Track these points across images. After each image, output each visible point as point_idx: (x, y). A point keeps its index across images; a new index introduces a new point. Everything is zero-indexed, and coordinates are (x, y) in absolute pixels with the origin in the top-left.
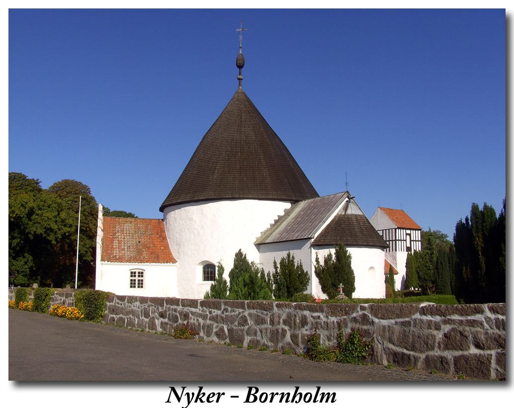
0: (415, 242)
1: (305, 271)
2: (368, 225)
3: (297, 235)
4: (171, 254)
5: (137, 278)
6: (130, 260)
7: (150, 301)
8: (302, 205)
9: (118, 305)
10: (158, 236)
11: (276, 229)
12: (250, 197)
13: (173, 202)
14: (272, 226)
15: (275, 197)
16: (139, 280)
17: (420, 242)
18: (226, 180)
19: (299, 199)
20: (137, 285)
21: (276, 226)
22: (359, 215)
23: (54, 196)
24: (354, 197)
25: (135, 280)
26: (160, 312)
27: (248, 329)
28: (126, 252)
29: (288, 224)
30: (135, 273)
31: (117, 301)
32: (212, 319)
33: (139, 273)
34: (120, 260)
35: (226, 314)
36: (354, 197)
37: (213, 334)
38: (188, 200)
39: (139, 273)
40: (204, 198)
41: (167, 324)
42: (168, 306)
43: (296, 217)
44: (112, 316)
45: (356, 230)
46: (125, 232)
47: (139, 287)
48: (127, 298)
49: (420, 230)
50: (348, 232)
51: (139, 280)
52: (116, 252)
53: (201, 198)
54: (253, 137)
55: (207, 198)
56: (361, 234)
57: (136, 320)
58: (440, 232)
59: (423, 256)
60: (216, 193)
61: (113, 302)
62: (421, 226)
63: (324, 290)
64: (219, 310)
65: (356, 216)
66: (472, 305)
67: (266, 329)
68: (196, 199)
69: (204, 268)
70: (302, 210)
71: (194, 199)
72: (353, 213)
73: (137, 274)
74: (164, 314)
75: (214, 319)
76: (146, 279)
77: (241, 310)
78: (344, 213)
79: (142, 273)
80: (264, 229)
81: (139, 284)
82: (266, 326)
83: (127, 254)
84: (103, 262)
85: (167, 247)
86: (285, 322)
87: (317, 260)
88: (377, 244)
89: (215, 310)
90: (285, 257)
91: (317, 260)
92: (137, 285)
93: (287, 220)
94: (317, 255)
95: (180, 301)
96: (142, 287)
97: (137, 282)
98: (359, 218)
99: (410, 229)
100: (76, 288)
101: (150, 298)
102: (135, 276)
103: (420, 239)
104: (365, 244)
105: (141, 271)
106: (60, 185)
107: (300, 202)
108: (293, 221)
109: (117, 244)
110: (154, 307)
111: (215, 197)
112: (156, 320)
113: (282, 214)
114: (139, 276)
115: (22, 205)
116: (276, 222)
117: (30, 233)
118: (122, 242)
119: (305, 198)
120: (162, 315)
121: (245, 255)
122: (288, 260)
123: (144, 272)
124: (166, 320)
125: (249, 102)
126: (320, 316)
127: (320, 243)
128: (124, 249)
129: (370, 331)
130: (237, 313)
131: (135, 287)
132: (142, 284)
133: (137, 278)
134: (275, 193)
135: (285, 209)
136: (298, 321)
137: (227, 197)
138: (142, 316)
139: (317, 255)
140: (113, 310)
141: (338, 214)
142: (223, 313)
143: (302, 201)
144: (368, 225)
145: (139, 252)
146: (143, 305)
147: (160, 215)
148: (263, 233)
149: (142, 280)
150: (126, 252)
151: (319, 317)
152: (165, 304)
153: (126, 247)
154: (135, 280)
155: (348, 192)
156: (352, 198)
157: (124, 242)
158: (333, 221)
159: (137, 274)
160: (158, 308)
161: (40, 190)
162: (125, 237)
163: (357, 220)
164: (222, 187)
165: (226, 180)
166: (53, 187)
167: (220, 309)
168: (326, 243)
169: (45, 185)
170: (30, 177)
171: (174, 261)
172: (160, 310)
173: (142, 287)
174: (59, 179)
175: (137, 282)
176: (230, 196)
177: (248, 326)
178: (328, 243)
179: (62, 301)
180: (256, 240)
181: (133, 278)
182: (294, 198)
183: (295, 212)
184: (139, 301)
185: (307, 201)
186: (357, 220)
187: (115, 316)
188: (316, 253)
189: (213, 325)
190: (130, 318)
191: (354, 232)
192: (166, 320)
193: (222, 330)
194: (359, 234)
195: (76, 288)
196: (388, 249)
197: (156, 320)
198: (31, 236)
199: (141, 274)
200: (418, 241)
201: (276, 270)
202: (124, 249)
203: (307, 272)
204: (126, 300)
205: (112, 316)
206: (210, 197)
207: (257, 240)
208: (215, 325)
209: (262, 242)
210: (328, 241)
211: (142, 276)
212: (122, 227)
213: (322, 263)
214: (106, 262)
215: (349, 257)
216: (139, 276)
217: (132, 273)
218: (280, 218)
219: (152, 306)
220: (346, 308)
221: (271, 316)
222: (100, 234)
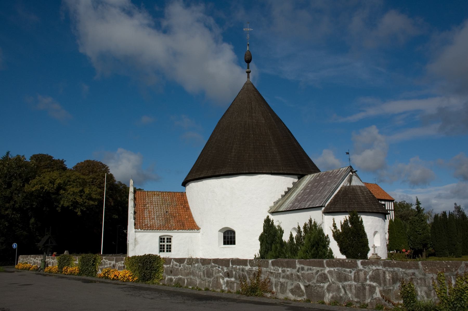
0: (391, 209)
1: (326, 235)
2: (370, 194)
3: (308, 204)
4: (195, 222)
5: (166, 244)
6: (159, 228)
7: (213, 262)
8: (308, 179)
9: (176, 267)
10: (182, 206)
11: (287, 199)
12: (264, 172)
13: (196, 177)
14: (283, 196)
15: (285, 172)
16: (167, 245)
17: (393, 211)
18: (242, 158)
19: (304, 173)
20: (165, 250)
21: (286, 197)
22: (362, 186)
23: (78, 174)
24: (357, 171)
25: (164, 245)
26: (225, 272)
27: (329, 286)
28: (156, 221)
29: (298, 195)
30: (164, 239)
31: (175, 263)
32: (287, 277)
33: (167, 239)
34: (151, 228)
35: (303, 272)
36: (357, 171)
37: (288, 291)
38: (209, 175)
39: (167, 239)
40: (224, 173)
41: (232, 283)
42: (234, 266)
43: (305, 189)
44: (169, 277)
45: (361, 199)
46: (154, 203)
47: (167, 251)
48: (186, 260)
49: (392, 201)
50: (354, 201)
51: (167, 245)
52: (147, 221)
53: (222, 173)
54: (263, 121)
55: (227, 173)
56: (366, 203)
57: (198, 281)
58: (405, 201)
59: (412, 222)
60: (235, 169)
61: (170, 264)
62: (393, 197)
63: (343, 251)
64: (293, 268)
65: (360, 187)
66: (238, 267)
67: (350, 286)
68: (217, 174)
69: (224, 233)
70: (309, 183)
71: (215, 174)
72: (357, 185)
73: (166, 240)
74: (230, 273)
75: (289, 277)
76: (174, 244)
77: (319, 269)
78: (349, 185)
79: (170, 239)
80: (276, 199)
81: (167, 248)
82: (349, 283)
83: (157, 222)
84: (137, 230)
85: (190, 216)
86: (373, 279)
87: (335, 226)
88: (380, 212)
89: (289, 269)
90: (307, 223)
91: (335, 226)
92: (165, 250)
93: (297, 191)
94: (334, 221)
95: (248, 261)
96: (170, 251)
97: (166, 247)
98: (362, 189)
99: (385, 200)
100: (102, 254)
101: (213, 259)
102: (164, 242)
103: (393, 209)
104: (371, 211)
105: (169, 237)
106: (83, 165)
107: (306, 176)
108: (302, 192)
109: (148, 214)
110: (217, 268)
111: (234, 172)
112: (221, 280)
113: (291, 186)
114: (167, 242)
115: (51, 182)
116: (286, 193)
117: (58, 206)
118: (152, 212)
119: (310, 173)
120: (228, 275)
121: (273, 221)
122: (311, 225)
123: (172, 238)
124: (233, 279)
125: (257, 91)
126: (415, 273)
127: (331, 211)
128: (154, 219)
129: (295, 286)
130: (315, 271)
131: (164, 251)
132: (170, 248)
133: (166, 244)
134: (285, 168)
135: (293, 182)
136: (388, 278)
137: (244, 172)
138: (204, 277)
139: (334, 221)
140: (171, 272)
141: (343, 185)
142: (298, 271)
143: (307, 175)
144: (370, 194)
145: (167, 221)
146: (205, 266)
147: (181, 189)
148: (276, 203)
149: (170, 245)
150: (156, 221)
151: (414, 274)
152: (231, 265)
153: (156, 217)
154: (164, 245)
155: (351, 167)
156: (355, 172)
157: (154, 213)
158: (339, 191)
159: (166, 240)
160: (222, 269)
161: (64, 169)
162: (154, 208)
163: (361, 191)
164: (239, 163)
165: (242, 158)
166: (76, 167)
167: (294, 267)
168: (336, 211)
169: (70, 165)
170: (56, 158)
171: (198, 229)
172: (225, 270)
173: (170, 251)
174: (82, 159)
175: (166, 247)
176: (247, 172)
177: (329, 283)
178: (339, 211)
179: (112, 265)
180: (270, 209)
181: (169, 244)
182: (301, 173)
183: (302, 184)
184: (201, 262)
185: (312, 175)
186: (361, 191)
187: (173, 277)
188: (333, 219)
189: (287, 283)
190: (191, 279)
191: (360, 201)
192: (233, 279)
193: (298, 287)
194: (364, 203)
195: (102, 254)
196: (389, 215)
197: (221, 280)
198: (59, 209)
199: (169, 240)
200: (392, 210)
201: (300, 234)
202: (154, 219)
203: (328, 235)
204: (186, 262)
205: (169, 277)
206: (230, 173)
207: (271, 209)
208: (290, 282)
209: (276, 211)
210: (338, 208)
211: (170, 242)
212: (151, 199)
213: (339, 227)
214: (139, 230)
215: (362, 221)
216: (167, 242)
217: (161, 239)
218: (289, 189)
219: (215, 267)
220: (447, 266)
221: (355, 273)
222: (131, 204)
